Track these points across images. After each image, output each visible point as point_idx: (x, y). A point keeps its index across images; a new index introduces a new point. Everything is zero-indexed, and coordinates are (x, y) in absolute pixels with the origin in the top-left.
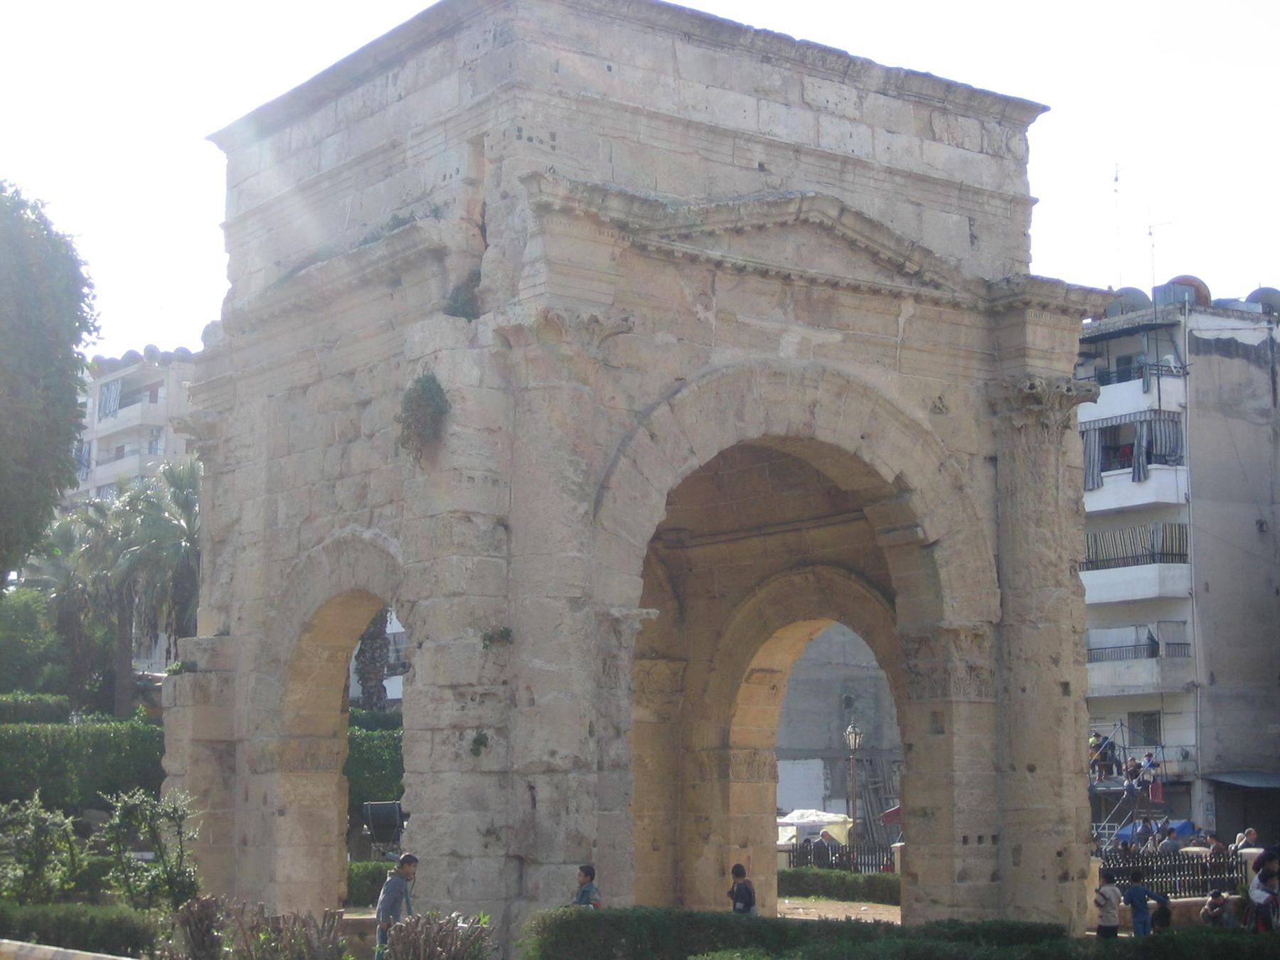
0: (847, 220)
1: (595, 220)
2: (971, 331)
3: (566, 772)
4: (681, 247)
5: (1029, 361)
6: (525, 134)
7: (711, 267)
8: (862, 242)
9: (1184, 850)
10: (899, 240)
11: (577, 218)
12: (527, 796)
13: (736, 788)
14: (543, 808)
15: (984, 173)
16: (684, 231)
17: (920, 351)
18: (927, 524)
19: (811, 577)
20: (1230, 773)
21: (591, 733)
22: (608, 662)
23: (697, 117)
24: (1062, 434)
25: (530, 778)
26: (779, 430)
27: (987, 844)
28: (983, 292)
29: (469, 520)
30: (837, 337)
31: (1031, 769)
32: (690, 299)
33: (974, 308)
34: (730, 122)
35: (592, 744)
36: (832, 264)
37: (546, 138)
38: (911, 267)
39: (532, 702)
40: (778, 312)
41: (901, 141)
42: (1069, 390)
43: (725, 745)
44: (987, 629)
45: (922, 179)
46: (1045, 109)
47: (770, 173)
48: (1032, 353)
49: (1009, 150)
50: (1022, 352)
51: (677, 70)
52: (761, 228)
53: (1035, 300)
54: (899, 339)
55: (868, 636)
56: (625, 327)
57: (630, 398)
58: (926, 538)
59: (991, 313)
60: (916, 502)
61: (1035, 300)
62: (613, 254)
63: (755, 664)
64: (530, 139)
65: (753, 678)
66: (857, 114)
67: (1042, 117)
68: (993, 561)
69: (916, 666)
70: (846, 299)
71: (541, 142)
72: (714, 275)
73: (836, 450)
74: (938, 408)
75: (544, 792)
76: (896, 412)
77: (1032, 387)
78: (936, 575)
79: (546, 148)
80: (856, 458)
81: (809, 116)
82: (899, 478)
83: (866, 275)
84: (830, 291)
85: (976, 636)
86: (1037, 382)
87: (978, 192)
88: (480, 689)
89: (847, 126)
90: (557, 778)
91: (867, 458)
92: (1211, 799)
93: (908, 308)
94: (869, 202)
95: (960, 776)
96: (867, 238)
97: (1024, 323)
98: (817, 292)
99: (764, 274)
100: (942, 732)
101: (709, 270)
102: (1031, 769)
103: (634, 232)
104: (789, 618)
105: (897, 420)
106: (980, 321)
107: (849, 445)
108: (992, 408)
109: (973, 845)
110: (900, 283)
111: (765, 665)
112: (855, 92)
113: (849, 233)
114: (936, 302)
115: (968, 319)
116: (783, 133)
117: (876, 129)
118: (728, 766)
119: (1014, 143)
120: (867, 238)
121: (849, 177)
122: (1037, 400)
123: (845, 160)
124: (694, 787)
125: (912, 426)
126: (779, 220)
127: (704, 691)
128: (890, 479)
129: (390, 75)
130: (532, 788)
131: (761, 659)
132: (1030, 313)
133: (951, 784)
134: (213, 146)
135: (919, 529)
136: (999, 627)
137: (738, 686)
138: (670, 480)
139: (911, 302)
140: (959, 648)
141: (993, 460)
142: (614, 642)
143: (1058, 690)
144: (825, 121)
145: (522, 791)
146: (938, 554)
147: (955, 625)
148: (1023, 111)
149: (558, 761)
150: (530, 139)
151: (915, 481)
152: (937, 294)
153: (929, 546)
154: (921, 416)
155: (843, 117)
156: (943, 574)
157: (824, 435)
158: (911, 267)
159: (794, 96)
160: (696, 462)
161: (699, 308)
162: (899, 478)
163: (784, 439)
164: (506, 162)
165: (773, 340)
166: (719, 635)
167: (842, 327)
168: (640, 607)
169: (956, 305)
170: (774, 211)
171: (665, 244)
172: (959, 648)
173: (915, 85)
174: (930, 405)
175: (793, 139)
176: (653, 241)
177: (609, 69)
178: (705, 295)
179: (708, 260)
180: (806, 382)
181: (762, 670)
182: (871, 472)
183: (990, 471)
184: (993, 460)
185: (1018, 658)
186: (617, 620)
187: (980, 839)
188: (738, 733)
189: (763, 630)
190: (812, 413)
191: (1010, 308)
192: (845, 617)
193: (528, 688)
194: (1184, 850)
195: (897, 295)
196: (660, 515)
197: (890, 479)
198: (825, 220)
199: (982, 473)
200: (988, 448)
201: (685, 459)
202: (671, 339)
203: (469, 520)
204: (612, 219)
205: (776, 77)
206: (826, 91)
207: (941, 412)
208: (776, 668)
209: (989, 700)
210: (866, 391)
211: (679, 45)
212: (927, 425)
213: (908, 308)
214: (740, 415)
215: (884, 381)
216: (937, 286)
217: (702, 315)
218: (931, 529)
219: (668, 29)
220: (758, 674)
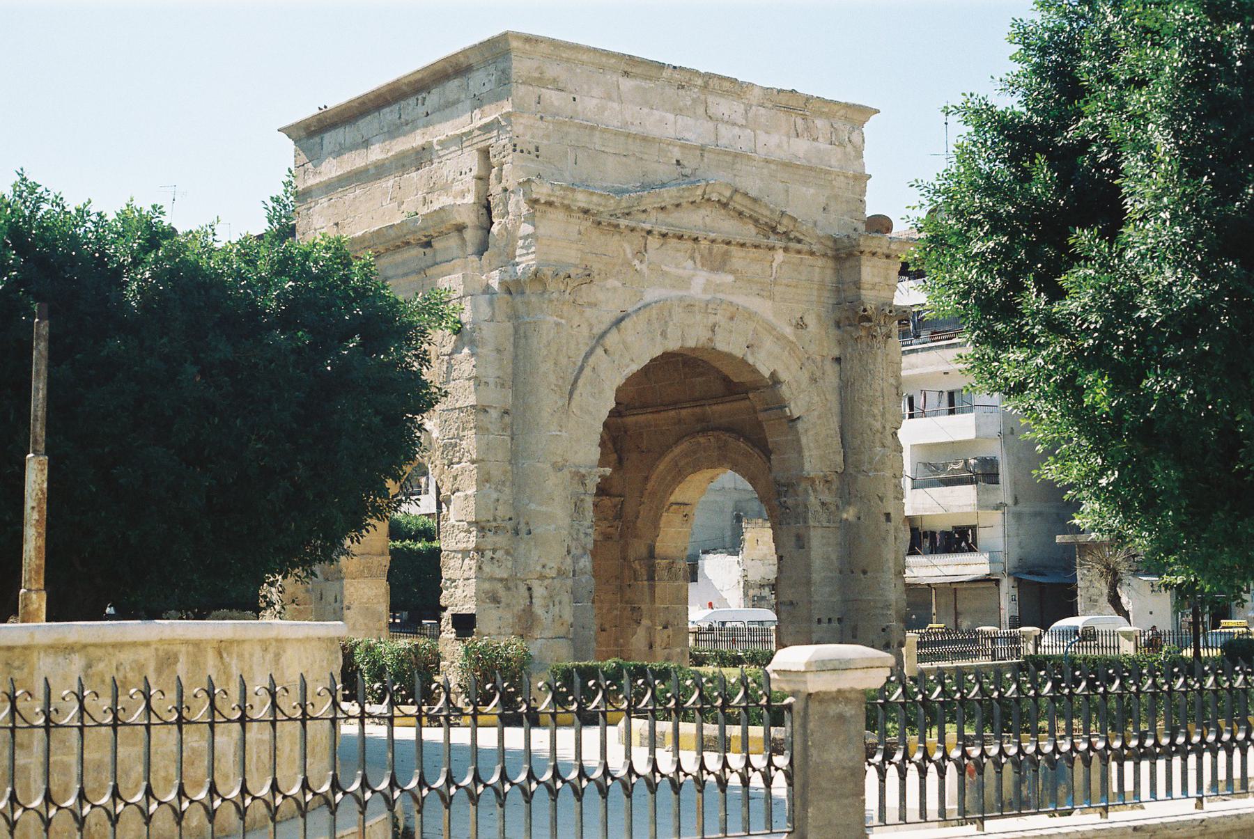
0: (738, 198)
1: (567, 208)
2: (820, 270)
3: (553, 578)
4: (623, 222)
5: (863, 292)
6: (518, 149)
7: (644, 234)
8: (747, 212)
9: (980, 628)
10: (772, 211)
11: (556, 207)
12: (526, 594)
13: (660, 586)
14: (537, 601)
15: (834, 157)
16: (626, 211)
17: (788, 286)
18: (792, 405)
19: (712, 439)
20: (1030, 573)
21: (569, 552)
22: (578, 507)
23: (633, 130)
24: (886, 343)
25: (528, 582)
26: (691, 343)
27: (835, 624)
28: (830, 244)
29: (486, 411)
30: (730, 278)
31: (865, 572)
32: (630, 256)
33: (825, 255)
34: (655, 132)
35: (569, 560)
36: (728, 226)
37: (533, 150)
38: (781, 229)
39: (529, 533)
40: (690, 263)
41: (774, 140)
42: (890, 312)
43: (651, 554)
44: (834, 476)
45: (787, 165)
46: (877, 111)
47: (684, 167)
48: (866, 286)
49: (850, 141)
50: (858, 284)
51: (620, 97)
52: (678, 205)
53: (867, 250)
54: (772, 278)
55: (752, 480)
56: (589, 277)
57: (591, 327)
58: (791, 416)
59: (837, 258)
60: (785, 391)
61: (867, 250)
62: (579, 231)
63: (672, 499)
64: (522, 151)
65: (672, 509)
66: (744, 122)
67: (873, 118)
68: (838, 430)
69: (785, 502)
70: (734, 250)
71: (529, 153)
72: (646, 239)
73: (729, 356)
74: (801, 325)
75: (539, 591)
76: (771, 329)
77: (865, 310)
78: (799, 441)
79: (532, 156)
80: (743, 362)
81: (711, 124)
82: (773, 374)
83: (749, 232)
84: (726, 247)
85: (827, 481)
86: (868, 307)
87: (828, 173)
88: (494, 524)
89: (736, 130)
90: (546, 582)
91: (751, 361)
92: (1015, 592)
93: (780, 256)
94: (752, 185)
95: (816, 577)
96: (751, 210)
97: (860, 266)
98: (719, 248)
99: (681, 237)
100: (802, 547)
101: (643, 237)
102: (865, 572)
103: (594, 215)
104: (697, 468)
105: (771, 334)
106: (830, 264)
107: (738, 352)
108: (838, 325)
109: (824, 625)
110: (773, 240)
111: (680, 501)
112: (742, 106)
113: (739, 207)
114: (799, 252)
115: (820, 262)
116: (693, 138)
117: (758, 132)
118: (654, 572)
119: (855, 137)
120: (751, 210)
121: (738, 166)
122: (869, 319)
123: (736, 155)
124: (630, 586)
125: (780, 338)
126: (690, 200)
127: (637, 517)
128: (767, 375)
129: (420, 97)
130: (529, 589)
131: (677, 496)
132: (863, 257)
133: (809, 583)
134: (284, 135)
135: (787, 409)
136: (842, 475)
137: (661, 515)
138: (619, 380)
139: (781, 251)
140: (815, 491)
141: (838, 360)
142: (582, 490)
143: (883, 519)
144: (723, 129)
145: (523, 590)
146: (800, 426)
147: (812, 475)
148: (859, 114)
149: (547, 572)
150: (522, 151)
151: (783, 376)
152: (799, 246)
153: (793, 420)
154: (788, 331)
155: (734, 124)
156: (804, 440)
157: (721, 346)
158: (781, 229)
159: (701, 111)
160: (635, 368)
161: (636, 262)
162: (773, 374)
163: (694, 349)
164: (505, 166)
165: (685, 282)
166: (647, 479)
167: (733, 272)
168: (598, 466)
169: (812, 253)
170: (686, 194)
171: (614, 221)
172: (815, 491)
173: (783, 99)
174: (794, 322)
175: (699, 142)
176: (605, 219)
177: (574, 99)
178: (641, 253)
179: (642, 230)
180: (709, 311)
181: (678, 504)
182: (754, 371)
183: (837, 368)
184: (838, 360)
185: (856, 496)
186: (584, 476)
187: (830, 620)
188: (660, 547)
189: (679, 475)
190: (713, 331)
191: (850, 255)
192: (735, 467)
193: (527, 524)
194: (980, 628)
195: (772, 248)
196: (612, 404)
197: (767, 375)
198: (722, 198)
199: (831, 370)
200: (836, 352)
201: (628, 366)
202: (618, 284)
203: (486, 411)
204: (579, 208)
205: (688, 98)
206: (723, 107)
207: (802, 328)
208: (686, 501)
209: (834, 525)
210: (751, 315)
211: (621, 79)
212: (792, 338)
213: (780, 256)
214: (664, 334)
215: (763, 307)
216: (799, 241)
217: (638, 267)
218: (795, 409)
219: (614, 70)
220: (674, 506)
